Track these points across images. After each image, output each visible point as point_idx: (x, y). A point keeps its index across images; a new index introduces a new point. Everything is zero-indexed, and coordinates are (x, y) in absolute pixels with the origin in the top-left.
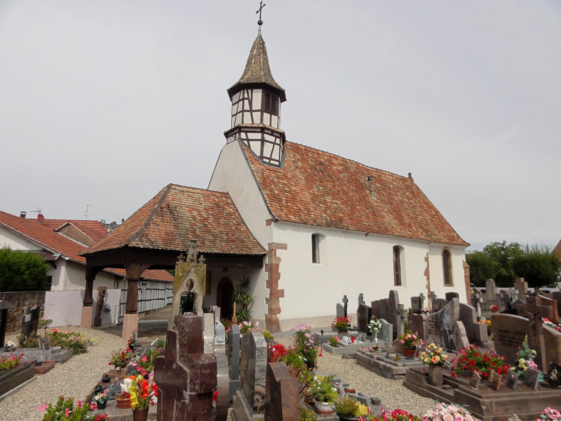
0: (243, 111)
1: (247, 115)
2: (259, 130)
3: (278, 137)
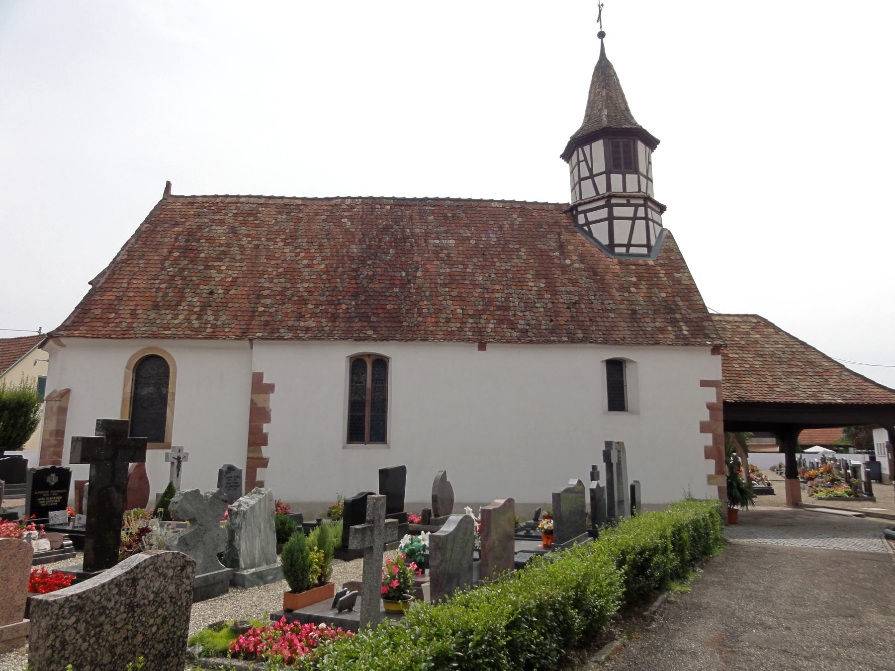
3: (641, 205)
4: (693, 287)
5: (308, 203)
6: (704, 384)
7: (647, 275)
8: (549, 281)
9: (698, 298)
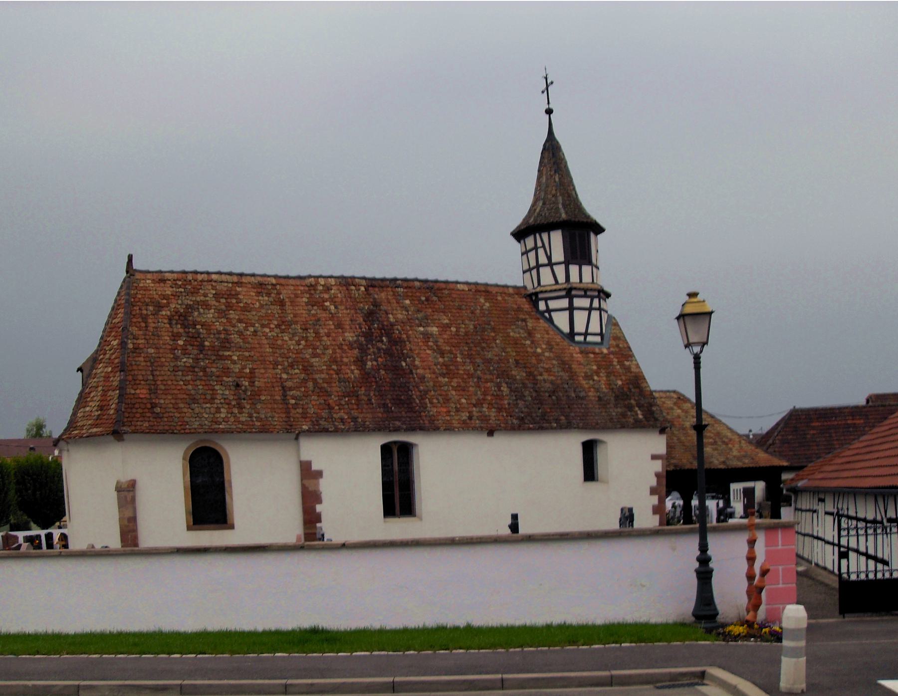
0: (538, 266)
1: (546, 273)
2: (563, 293)
3: (596, 297)
4: (641, 374)
5: (282, 281)
6: (654, 457)
7: (604, 363)
8: (528, 370)
9: (645, 385)
